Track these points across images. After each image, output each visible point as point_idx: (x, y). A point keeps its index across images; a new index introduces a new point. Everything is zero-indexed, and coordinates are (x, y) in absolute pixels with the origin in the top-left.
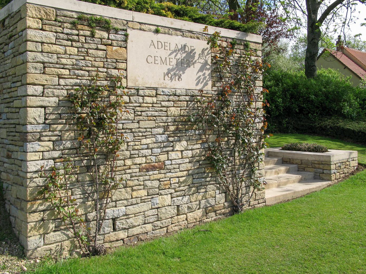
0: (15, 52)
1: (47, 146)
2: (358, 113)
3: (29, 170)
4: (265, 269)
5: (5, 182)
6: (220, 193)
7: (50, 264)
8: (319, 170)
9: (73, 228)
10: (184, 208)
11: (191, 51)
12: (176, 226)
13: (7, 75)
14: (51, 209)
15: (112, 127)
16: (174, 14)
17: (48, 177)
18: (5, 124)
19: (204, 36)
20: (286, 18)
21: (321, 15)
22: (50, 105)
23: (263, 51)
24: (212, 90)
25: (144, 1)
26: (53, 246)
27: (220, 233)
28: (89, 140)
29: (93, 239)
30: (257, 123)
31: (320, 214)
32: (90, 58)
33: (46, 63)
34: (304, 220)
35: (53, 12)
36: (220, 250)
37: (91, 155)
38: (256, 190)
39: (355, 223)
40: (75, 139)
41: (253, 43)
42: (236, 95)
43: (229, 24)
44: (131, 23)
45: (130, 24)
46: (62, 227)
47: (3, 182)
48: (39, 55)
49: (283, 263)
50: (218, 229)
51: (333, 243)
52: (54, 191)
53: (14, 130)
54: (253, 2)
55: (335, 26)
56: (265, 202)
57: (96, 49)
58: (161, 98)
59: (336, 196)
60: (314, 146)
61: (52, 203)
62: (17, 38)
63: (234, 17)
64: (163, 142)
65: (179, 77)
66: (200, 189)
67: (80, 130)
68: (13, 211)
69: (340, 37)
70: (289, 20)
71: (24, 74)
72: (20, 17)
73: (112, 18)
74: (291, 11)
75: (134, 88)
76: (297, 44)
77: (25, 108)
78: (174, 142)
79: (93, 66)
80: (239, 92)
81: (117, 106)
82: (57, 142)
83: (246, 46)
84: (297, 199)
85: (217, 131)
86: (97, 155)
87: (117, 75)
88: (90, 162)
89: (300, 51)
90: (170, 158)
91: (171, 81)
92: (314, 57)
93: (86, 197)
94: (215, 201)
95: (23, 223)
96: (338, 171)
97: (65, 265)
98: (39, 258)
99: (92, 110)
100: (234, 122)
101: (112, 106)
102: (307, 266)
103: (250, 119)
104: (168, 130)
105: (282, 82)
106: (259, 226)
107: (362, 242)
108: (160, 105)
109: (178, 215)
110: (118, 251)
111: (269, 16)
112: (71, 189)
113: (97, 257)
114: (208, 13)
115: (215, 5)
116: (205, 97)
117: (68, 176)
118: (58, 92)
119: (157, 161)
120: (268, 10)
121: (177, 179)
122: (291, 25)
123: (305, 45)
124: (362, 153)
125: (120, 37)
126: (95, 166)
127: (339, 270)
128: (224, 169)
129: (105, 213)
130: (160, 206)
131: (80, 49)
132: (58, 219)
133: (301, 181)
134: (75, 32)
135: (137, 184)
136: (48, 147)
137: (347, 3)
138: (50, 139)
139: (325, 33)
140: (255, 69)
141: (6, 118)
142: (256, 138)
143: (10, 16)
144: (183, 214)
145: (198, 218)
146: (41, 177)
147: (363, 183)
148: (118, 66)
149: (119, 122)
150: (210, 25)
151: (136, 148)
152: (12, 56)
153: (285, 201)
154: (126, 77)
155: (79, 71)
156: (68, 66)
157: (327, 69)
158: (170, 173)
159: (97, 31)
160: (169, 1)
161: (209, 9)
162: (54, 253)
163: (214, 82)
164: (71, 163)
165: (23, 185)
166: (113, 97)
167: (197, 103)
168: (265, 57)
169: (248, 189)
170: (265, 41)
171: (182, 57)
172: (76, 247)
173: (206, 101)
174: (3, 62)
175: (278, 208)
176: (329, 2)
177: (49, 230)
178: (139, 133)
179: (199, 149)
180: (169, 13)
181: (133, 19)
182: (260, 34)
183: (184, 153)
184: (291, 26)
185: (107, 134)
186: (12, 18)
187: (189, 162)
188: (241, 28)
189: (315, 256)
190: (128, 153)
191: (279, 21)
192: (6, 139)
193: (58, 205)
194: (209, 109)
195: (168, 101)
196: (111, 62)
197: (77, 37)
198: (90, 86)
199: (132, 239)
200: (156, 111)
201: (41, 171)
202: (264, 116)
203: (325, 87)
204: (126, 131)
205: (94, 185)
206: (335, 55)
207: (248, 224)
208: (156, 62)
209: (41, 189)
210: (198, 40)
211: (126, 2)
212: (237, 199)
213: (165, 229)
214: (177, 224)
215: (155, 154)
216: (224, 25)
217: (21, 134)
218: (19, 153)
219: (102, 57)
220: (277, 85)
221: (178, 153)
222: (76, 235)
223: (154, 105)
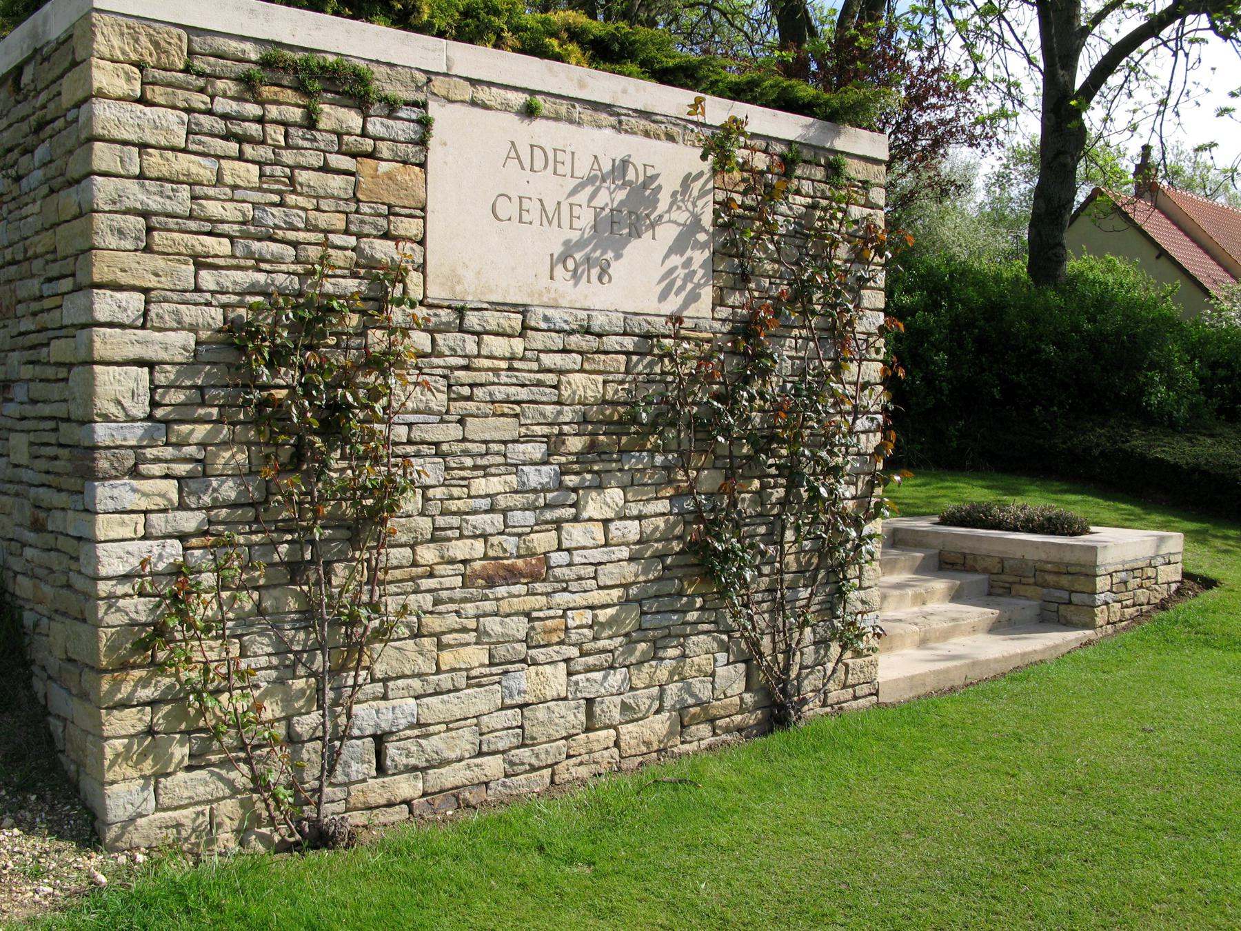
0: (54, 178)
1: (159, 495)
2: (1193, 407)
3: (103, 571)
4: (864, 902)
5: (27, 607)
6: (728, 664)
7: (178, 869)
8: (1057, 593)
9: (248, 761)
10: (610, 709)
11: (644, 182)
12: (581, 764)
13: (30, 253)
14: (175, 698)
15: (372, 434)
16: (589, 53)
17: (163, 597)
18: (23, 418)
19: (692, 131)
20: (973, 79)
21: (1088, 74)
22: (167, 358)
23: (889, 188)
24: (714, 319)
25: (487, 6)
26: (186, 815)
27: (724, 790)
28: (296, 478)
29: (312, 796)
30: (863, 432)
31: (1052, 734)
32: (301, 201)
33: (156, 214)
34: (1000, 753)
35: (180, 39)
36: (723, 841)
37: (303, 528)
38: (848, 654)
39: (1159, 762)
40: (251, 473)
41: (856, 161)
42: (796, 338)
43: (777, 90)
44: (443, 82)
45: (438, 84)
46: (213, 758)
47: (22, 607)
48: (132, 186)
49: (923, 884)
50: (721, 778)
51: (1085, 823)
52: (184, 640)
53: (51, 438)
54: (861, 18)
55: (1134, 111)
56: (877, 694)
57: (320, 169)
58: (538, 340)
59: (1105, 676)
60: (1046, 513)
61: (178, 680)
62: (60, 131)
63: (797, 70)
64: (545, 489)
65: (604, 272)
66: (665, 648)
67: (267, 444)
68: (59, 699)
69: (1146, 149)
70: (980, 84)
71: (84, 252)
72: (70, 58)
73: (378, 62)
74: (987, 56)
75: (446, 303)
76: (1006, 167)
77: (87, 367)
78: (581, 492)
79: (310, 227)
80: (803, 327)
81: (391, 365)
82: (191, 482)
83: (834, 170)
84: (981, 685)
85: (725, 457)
86: (324, 527)
87: (393, 259)
88: (302, 550)
89: (1014, 192)
90: (566, 544)
91: (576, 285)
92: (1061, 216)
93: (288, 662)
94: (714, 689)
95: (90, 738)
96: (1119, 597)
97: (225, 874)
98: (143, 849)
99: (308, 375)
100: (784, 428)
101: (374, 363)
102: (998, 894)
103: (838, 418)
104: (562, 450)
105: (949, 295)
106: (854, 771)
107: (1174, 820)
108: (535, 366)
109: (588, 730)
110: (394, 837)
111: (915, 70)
112: (239, 637)
113: (326, 853)
114: (706, 51)
115: (732, 25)
116: (688, 339)
117: (228, 593)
118: (193, 313)
119: (522, 552)
120: (913, 49)
121: (589, 613)
122: (987, 102)
123: (1032, 173)
124: (1197, 541)
125: (403, 129)
126: (317, 564)
127: (1098, 906)
128: (745, 585)
129: (349, 717)
130: (529, 698)
131: (268, 170)
132: (200, 730)
133: (996, 628)
134: (253, 109)
135: (457, 627)
136: (163, 496)
137: (1174, 36)
138: (169, 472)
139: (1100, 136)
140: (862, 250)
141: (26, 399)
142: (855, 484)
143: (38, 55)
144: (607, 727)
145: (654, 739)
146: (140, 595)
147: (1193, 636)
148: (396, 229)
149: (395, 419)
150: (713, 93)
151: (454, 508)
152: (45, 189)
153: (941, 692)
154: (422, 268)
155: (265, 244)
156: (226, 228)
157: (1101, 256)
158: (566, 594)
159: (326, 108)
160: (573, 8)
161: (712, 36)
162: (190, 835)
163: (721, 289)
164: (238, 550)
165: (85, 618)
166: (379, 333)
167: (663, 362)
168: (895, 210)
169: (822, 652)
170: (899, 153)
171: (612, 201)
172: (257, 820)
173: (691, 354)
174: (16, 212)
175: (918, 712)
176: (1117, 31)
177: (173, 766)
178: (463, 459)
179: (663, 514)
180: (573, 47)
181: (448, 68)
182: (882, 131)
183: (612, 526)
184: (989, 105)
185: (359, 458)
186: (46, 64)
187: (631, 559)
188: (819, 105)
189: (1025, 865)
190: (425, 524)
191: (948, 88)
192: (27, 467)
193: (199, 686)
194: (701, 383)
195: (565, 351)
196: (371, 215)
197: (259, 127)
198: (300, 294)
199: (437, 802)
200: (523, 386)
201: (141, 576)
202: (885, 410)
203: (1092, 320)
204: (419, 451)
205: (314, 627)
206: (1128, 209)
207: (817, 763)
208: (526, 217)
209: (144, 635)
210: (670, 145)
211: (426, 9)
212: (785, 682)
213: (547, 773)
214: (586, 757)
215: (515, 530)
216: (762, 94)
217: (75, 451)
218: (70, 514)
219: (343, 195)
220: (933, 307)
221: (593, 529)
222: (259, 783)
223: (516, 364)
